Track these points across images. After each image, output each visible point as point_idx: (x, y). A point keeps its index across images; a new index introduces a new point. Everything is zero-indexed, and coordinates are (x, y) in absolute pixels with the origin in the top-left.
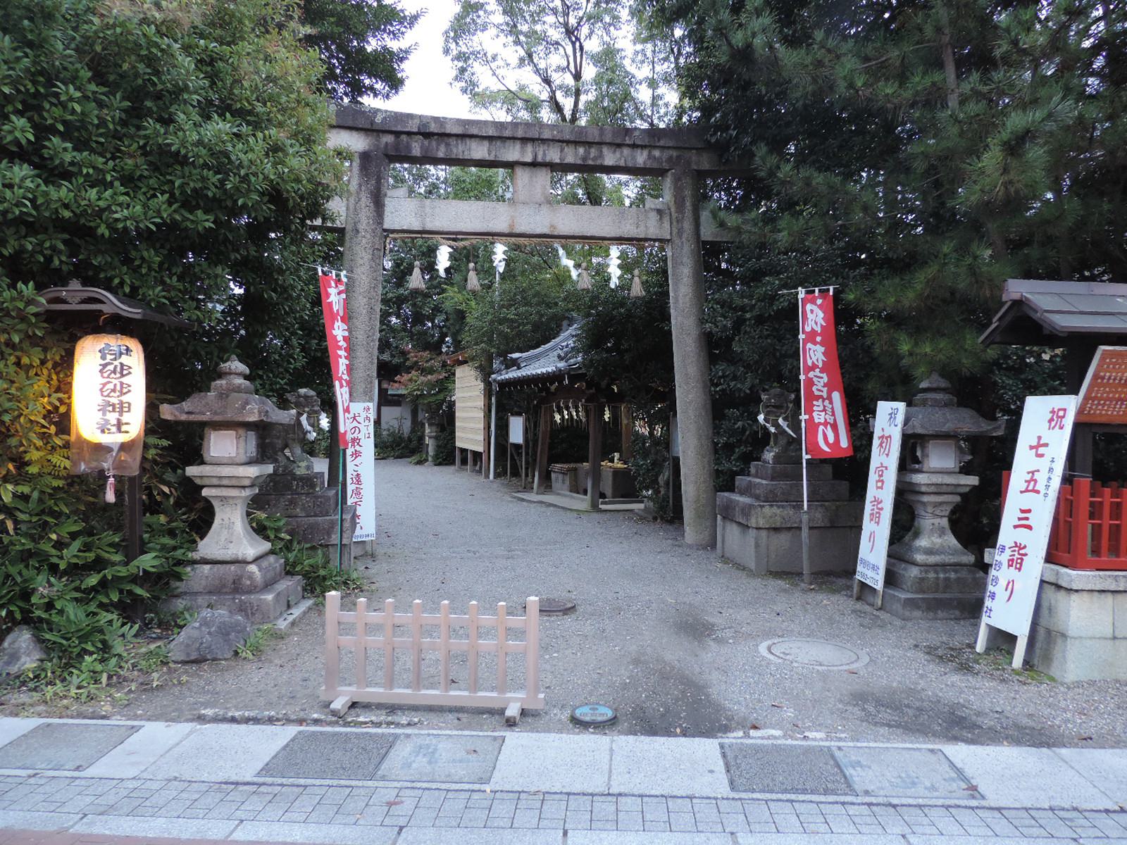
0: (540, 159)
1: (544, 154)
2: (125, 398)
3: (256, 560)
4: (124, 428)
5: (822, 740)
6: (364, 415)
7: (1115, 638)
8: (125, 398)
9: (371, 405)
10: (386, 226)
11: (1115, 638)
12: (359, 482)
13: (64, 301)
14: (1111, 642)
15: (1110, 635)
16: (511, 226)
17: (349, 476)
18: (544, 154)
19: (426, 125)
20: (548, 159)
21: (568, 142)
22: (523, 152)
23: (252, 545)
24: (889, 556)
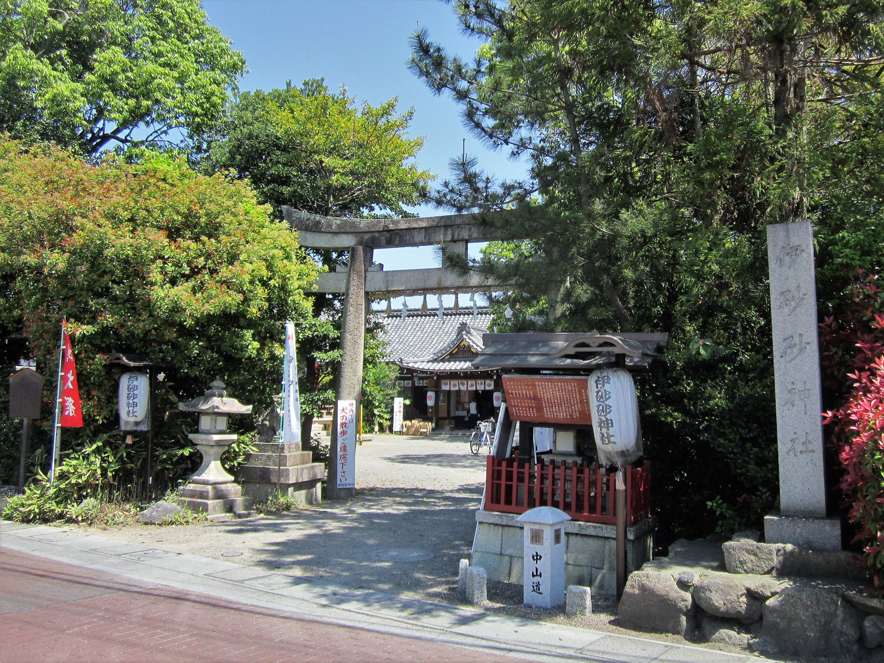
0: (456, 238)
4: (612, 439)
6: (349, 408)
11: (501, 554)
13: (588, 346)
15: (498, 551)
24: (534, 506)
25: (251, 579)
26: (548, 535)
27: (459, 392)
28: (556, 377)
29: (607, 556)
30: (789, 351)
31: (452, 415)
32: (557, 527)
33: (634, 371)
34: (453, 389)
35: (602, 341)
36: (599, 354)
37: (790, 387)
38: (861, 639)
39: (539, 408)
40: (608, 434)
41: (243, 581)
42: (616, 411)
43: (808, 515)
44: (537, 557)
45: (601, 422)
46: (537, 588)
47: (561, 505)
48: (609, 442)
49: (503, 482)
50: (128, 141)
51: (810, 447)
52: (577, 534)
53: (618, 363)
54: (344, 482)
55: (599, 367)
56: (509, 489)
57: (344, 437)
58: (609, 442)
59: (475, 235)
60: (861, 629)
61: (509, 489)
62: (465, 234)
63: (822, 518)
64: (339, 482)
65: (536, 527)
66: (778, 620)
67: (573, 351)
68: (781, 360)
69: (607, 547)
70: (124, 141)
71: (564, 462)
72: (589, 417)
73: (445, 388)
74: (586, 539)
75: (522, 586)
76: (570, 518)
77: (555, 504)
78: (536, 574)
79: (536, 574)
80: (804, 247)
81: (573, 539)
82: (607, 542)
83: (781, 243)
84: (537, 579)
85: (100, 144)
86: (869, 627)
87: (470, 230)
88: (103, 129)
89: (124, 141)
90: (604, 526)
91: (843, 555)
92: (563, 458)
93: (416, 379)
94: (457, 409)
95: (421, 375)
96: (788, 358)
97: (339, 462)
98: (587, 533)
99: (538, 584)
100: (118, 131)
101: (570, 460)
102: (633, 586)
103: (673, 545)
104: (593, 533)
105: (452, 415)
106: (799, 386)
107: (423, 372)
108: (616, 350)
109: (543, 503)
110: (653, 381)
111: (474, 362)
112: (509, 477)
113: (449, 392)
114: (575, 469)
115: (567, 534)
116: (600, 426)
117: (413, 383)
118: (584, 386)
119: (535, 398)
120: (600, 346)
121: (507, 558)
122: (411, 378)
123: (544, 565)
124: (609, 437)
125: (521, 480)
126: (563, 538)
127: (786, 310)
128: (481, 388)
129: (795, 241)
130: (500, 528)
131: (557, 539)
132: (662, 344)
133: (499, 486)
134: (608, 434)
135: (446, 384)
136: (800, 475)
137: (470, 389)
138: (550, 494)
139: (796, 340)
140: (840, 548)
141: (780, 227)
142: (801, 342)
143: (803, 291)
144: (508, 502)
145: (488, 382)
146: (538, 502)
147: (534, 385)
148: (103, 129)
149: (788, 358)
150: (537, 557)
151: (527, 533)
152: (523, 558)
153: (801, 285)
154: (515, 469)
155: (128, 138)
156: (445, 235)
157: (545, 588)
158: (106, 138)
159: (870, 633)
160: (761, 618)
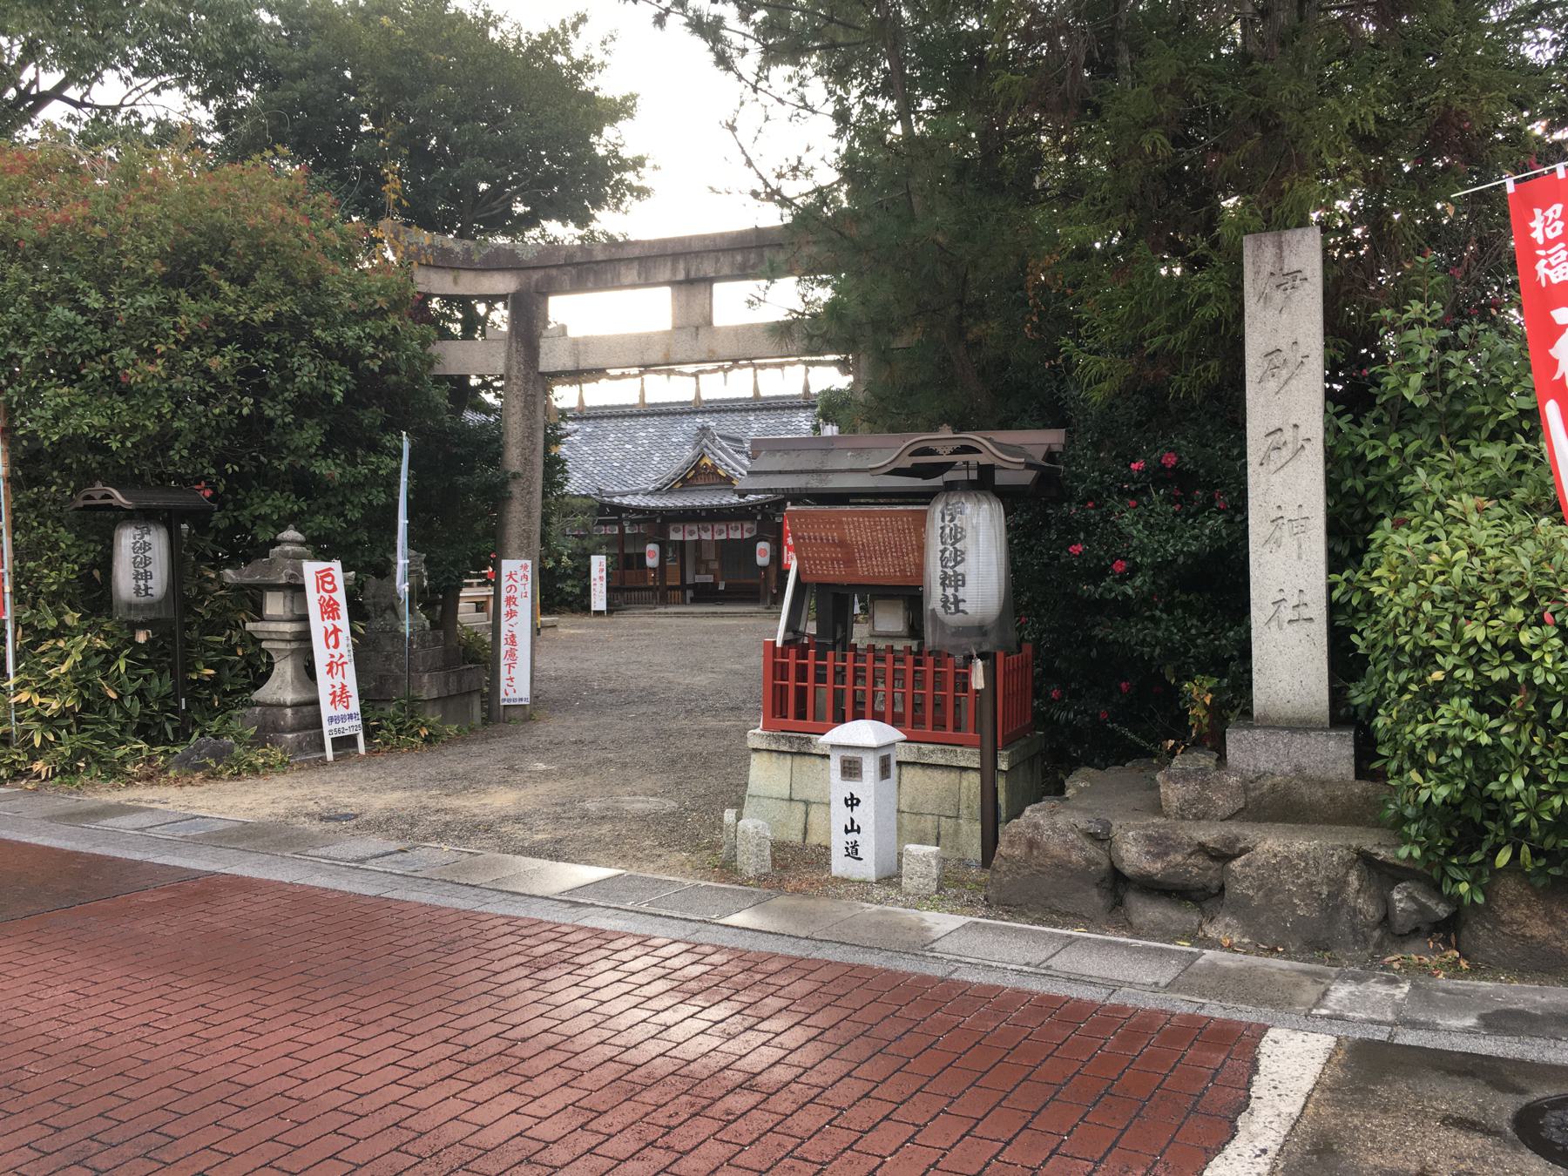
0: (693, 274)
1: (698, 269)
2: (959, 569)
3: (294, 705)
4: (962, 606)
5: (1468, 1031)
6: (521, 573)
7: (791, 800)
8: (959, 569)
9: (529, 563)
10: (541, 369)
11: (791, 800)
12: (513, 642)
13: (932, 452)
14: (785, 805)
15: (786, 794)
16: (667, 355)
17: (503, 637)
18: (698, 269)
19: (572, 256)
20: (701, 274)
21: (723, 250)
22: (674, 270)
23: (295, 690)
24: (844, 722)
25: (376, 857)
26: (870, 766)
27: (698, 542)
28: (876, 508)
29: (964, 798)
30: (1274, 455)
31: (689, 581)
32: (885, 753)
33: (1009, 497)
34: (688, 538)
35: (958, 444)
36: (949, 466)
37: (1276, 514)
38: (1386, 920)
39: (850, 561)
40: (955, 597)
41: (363, 860)
42: (971, 558)
43: (1299, 726)
44: (852, 802)
45: (945, 577)
46: (853, 851)
47: (889, 716)
48: (957, 610)
49: (791, 683)
50: (88, 105)
51: (1306, 613)
52: (914, 764)
53: (983, 483)
54: (512, 695)
55: (950, 487)
56: (801, 694)
57: (512, 621)
58: (957, 610)
59: (726, 270)
60: (1387, 903)
61: (801, 694)
62: (708, 269)
63: (1323, 729)
64: (502, 695)
65: (850, 754)
66: (1251, 893)
67: (907, 462)
68: (1260, 469)
69: (965, 783)
70: (79, 105)
71: (891, 649)
72: (920, 567)
73: (675, 536)
74: (929, 772)
75: (828, 848)
76: (904, 737)
77: (878, 716)
78: (852, 828)
79: (852, 828)
80: (1308, 273)
81: (908, 773)
82: (965, 775)
83: (1269, 268)
84: (852, 837)
85: (34, 110)
86: (1400, 901)
87: (717, 260)
88: (35, 82)
89: (79, 105)
90: (959, 749)
91: (1359, 788)
92: (890, 643)
93: (626, 524)
94: (698, 573)
95: (634, 516)
96: (1272, 467)
97: (503, 662)
98: (930, 761)
99: (855, 845)
100: (63, 85)
101: (899, 646)
102: (1011, 843)
103: (1072, 778)
104: (942, 762)
105: (689, 581)
106: (1290, 513)
107: (637, 510)
108: (983, 459)
109: (858, 716)
110: (1033, 514)
111: (1484, 849)
112: (802, 673)
113: (683, 543)
114: (910, 658)
115: (900, 764)
116: (943, 584)
117: (622, 530)
118: (921, 521)
119: (842, 544)
120: (955, 452)
121: (802, 807)
122: (619, 522)
123: (864, 815)
124: (957, 601)
125: (821, 678)
126: (894, 770)
127: (1272, 384)
128: (736, 535)
129: (1292, 263)
130: (789, 757)
131: (885, 771)
132: (1057, 448)
133: (784, 689)
134: (955, 597)
135: (677, 531)
136: (1288, 657)
137: (717, 537)
138: (868, 701)
139: (1288, 434)
140: (1352, 777)
141: (1268, 239)
142: (1295, 438)
143: (1303, 350)
144: (801, 715)
145: (747, 525)
146: (849, 713)
147: (841, 522)
148: (35, 82)
149: (1272, 467)
150: (852, 802)
151: (835, 764)
152: (829, 804)
153: (1300, 340)
154: (810, 662)
155: (87, 100)
156: (674, 270)
157: (868, 844)
158: (43, 99)
159: (1403, 910)
160: (1222, 889)
